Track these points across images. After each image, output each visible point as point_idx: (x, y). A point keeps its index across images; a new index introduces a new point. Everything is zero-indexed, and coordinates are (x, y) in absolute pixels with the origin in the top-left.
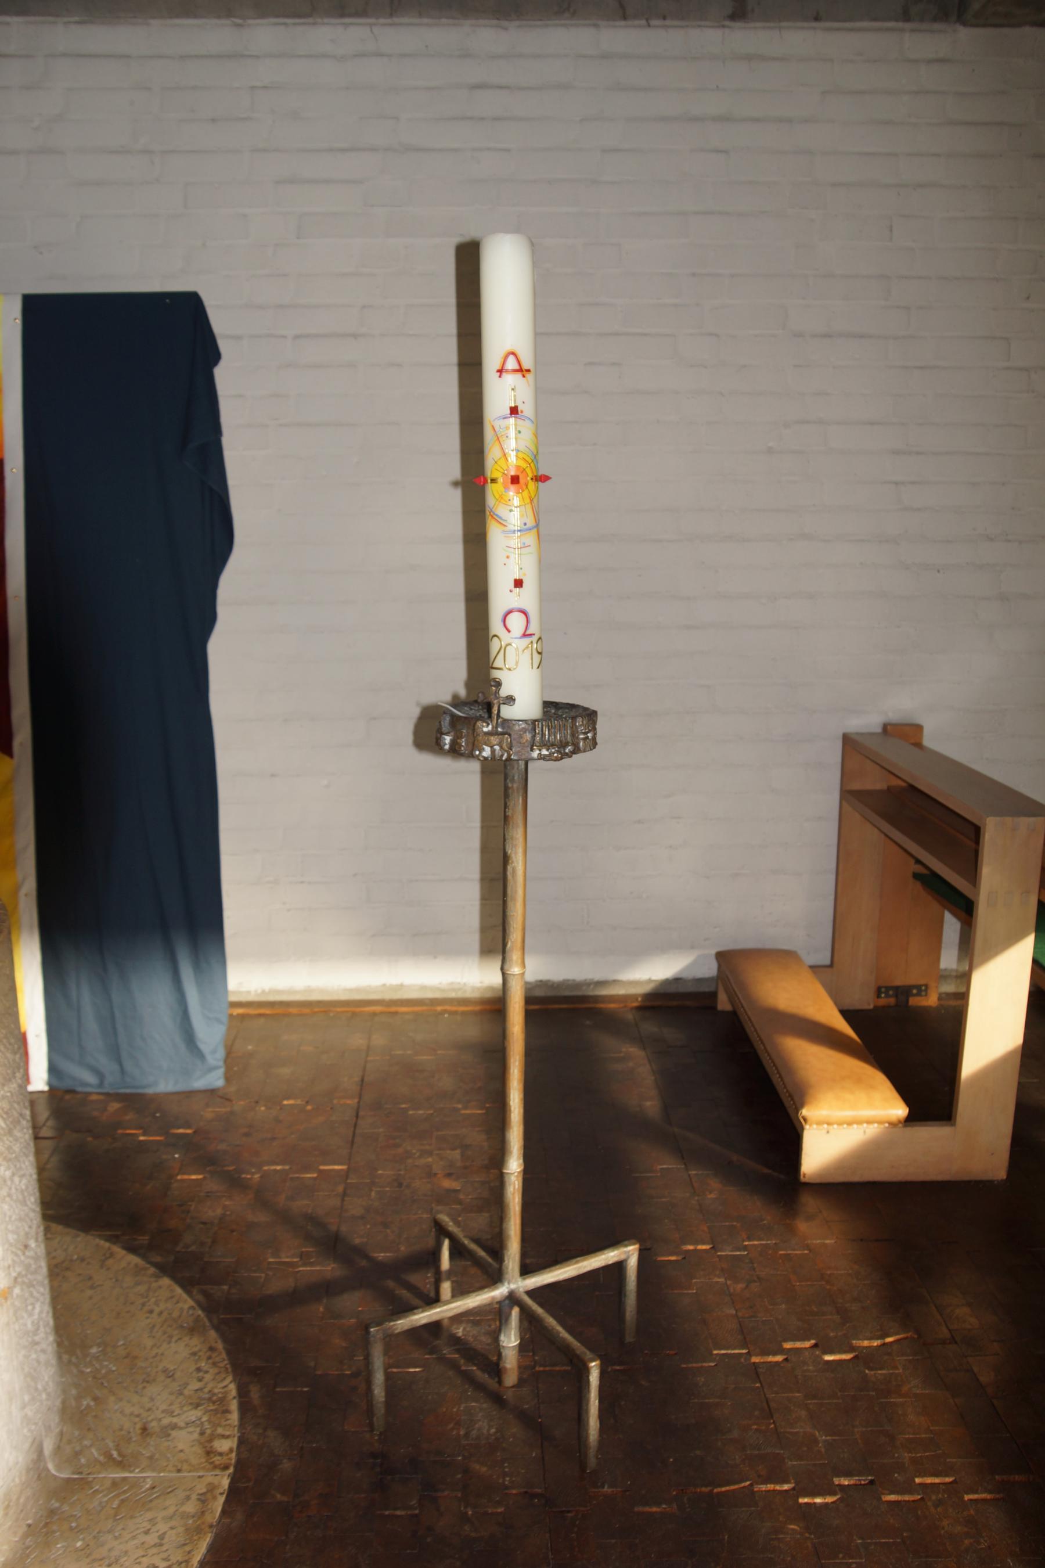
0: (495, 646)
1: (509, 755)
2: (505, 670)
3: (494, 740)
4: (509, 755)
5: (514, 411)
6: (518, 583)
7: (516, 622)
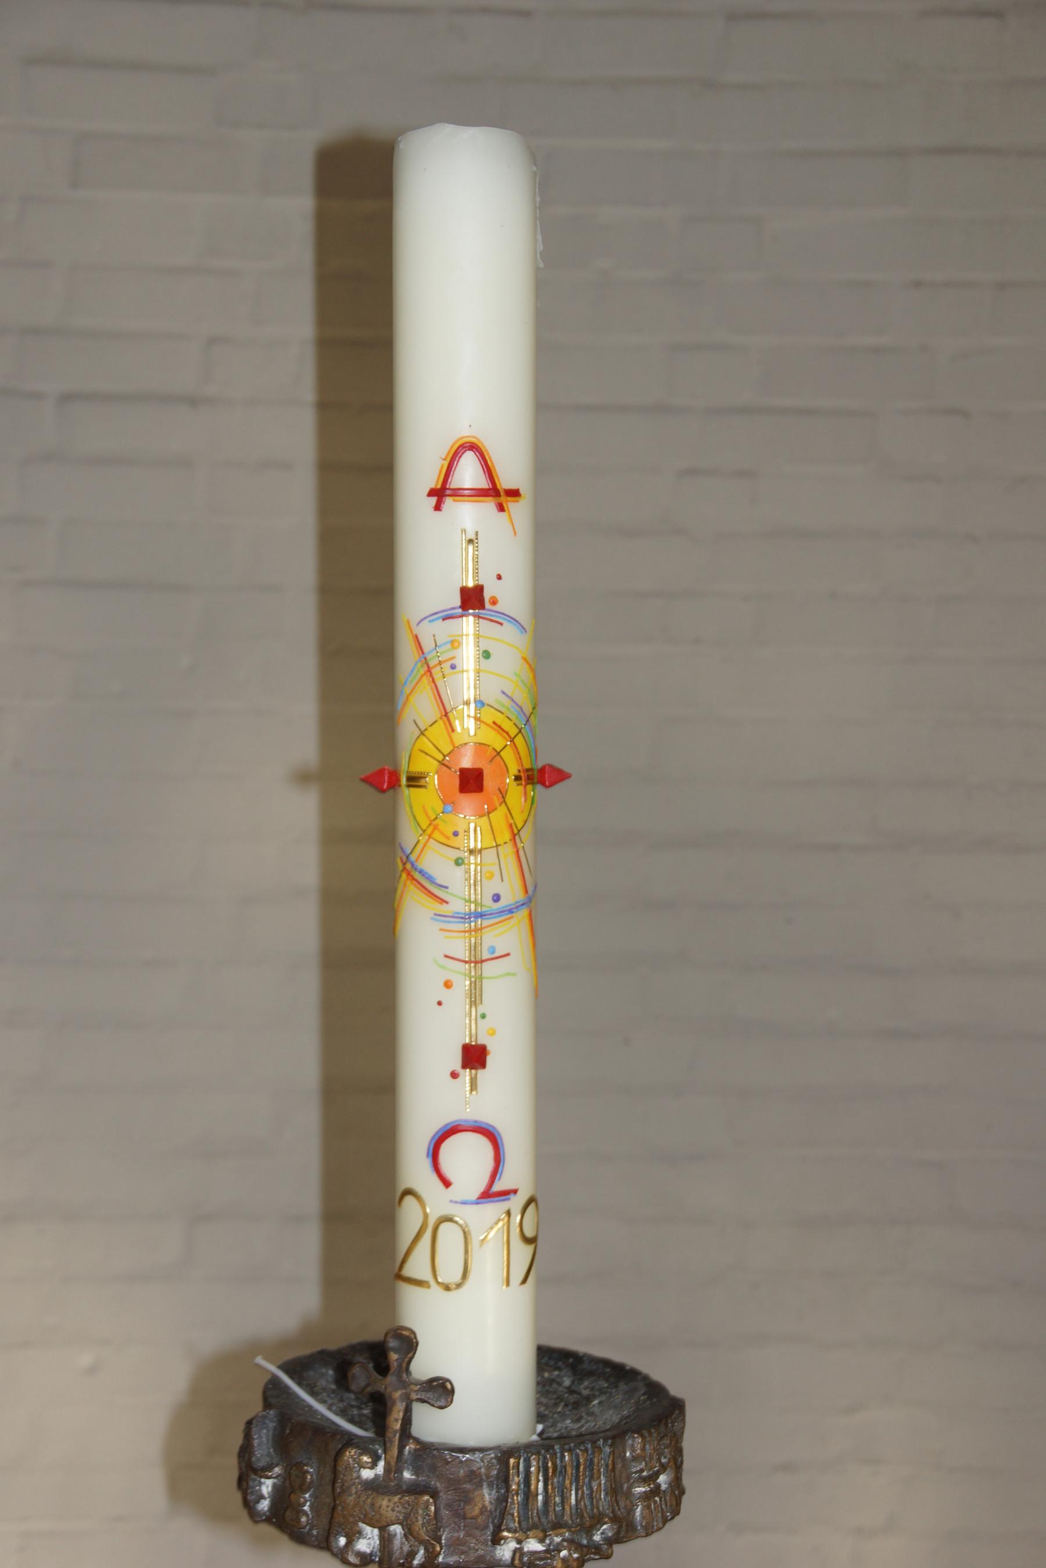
0: (410, 1216)
1: (431, 1556)
2: (435, 1290)
3: (387, 1505)
4: (431, 1556)
5: (472, 599)
6: (474, 1056)
7: (468, 1159)
